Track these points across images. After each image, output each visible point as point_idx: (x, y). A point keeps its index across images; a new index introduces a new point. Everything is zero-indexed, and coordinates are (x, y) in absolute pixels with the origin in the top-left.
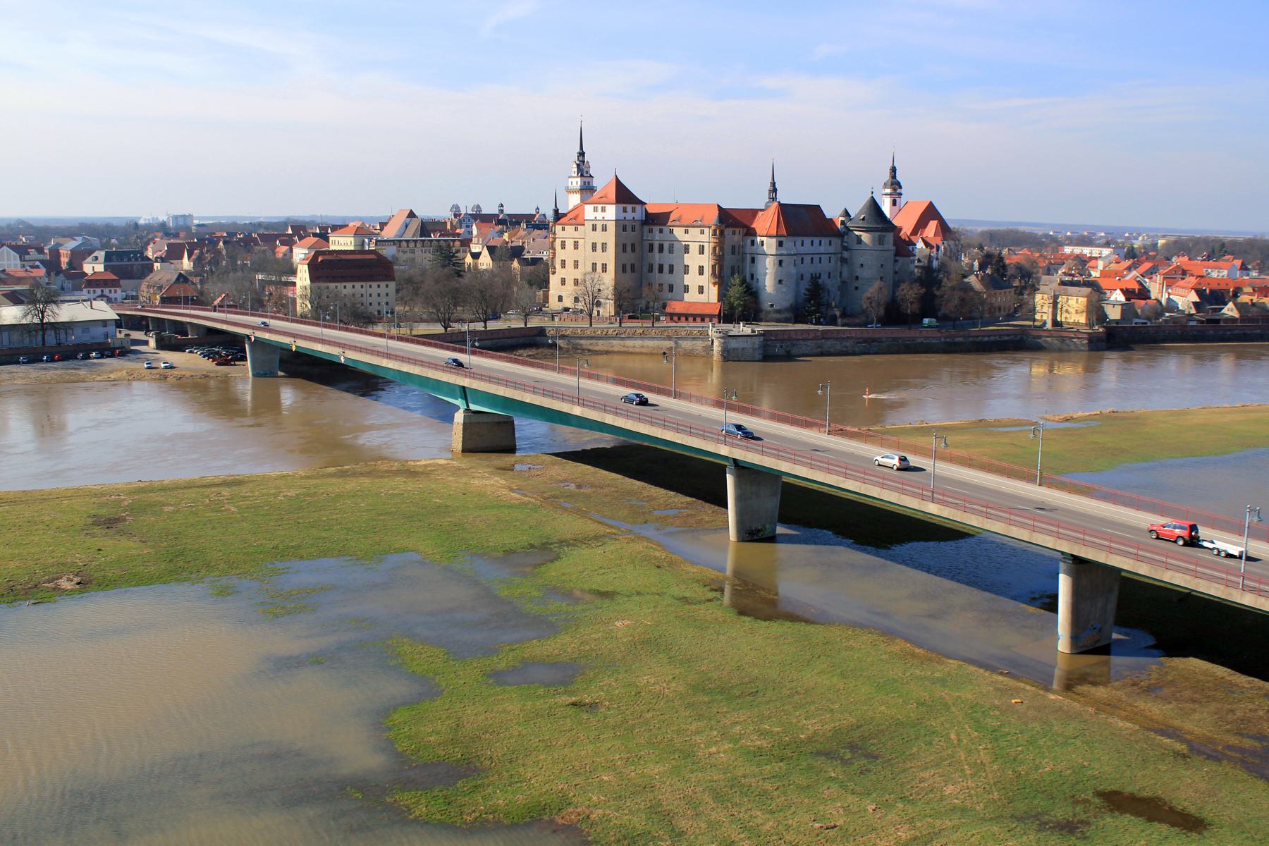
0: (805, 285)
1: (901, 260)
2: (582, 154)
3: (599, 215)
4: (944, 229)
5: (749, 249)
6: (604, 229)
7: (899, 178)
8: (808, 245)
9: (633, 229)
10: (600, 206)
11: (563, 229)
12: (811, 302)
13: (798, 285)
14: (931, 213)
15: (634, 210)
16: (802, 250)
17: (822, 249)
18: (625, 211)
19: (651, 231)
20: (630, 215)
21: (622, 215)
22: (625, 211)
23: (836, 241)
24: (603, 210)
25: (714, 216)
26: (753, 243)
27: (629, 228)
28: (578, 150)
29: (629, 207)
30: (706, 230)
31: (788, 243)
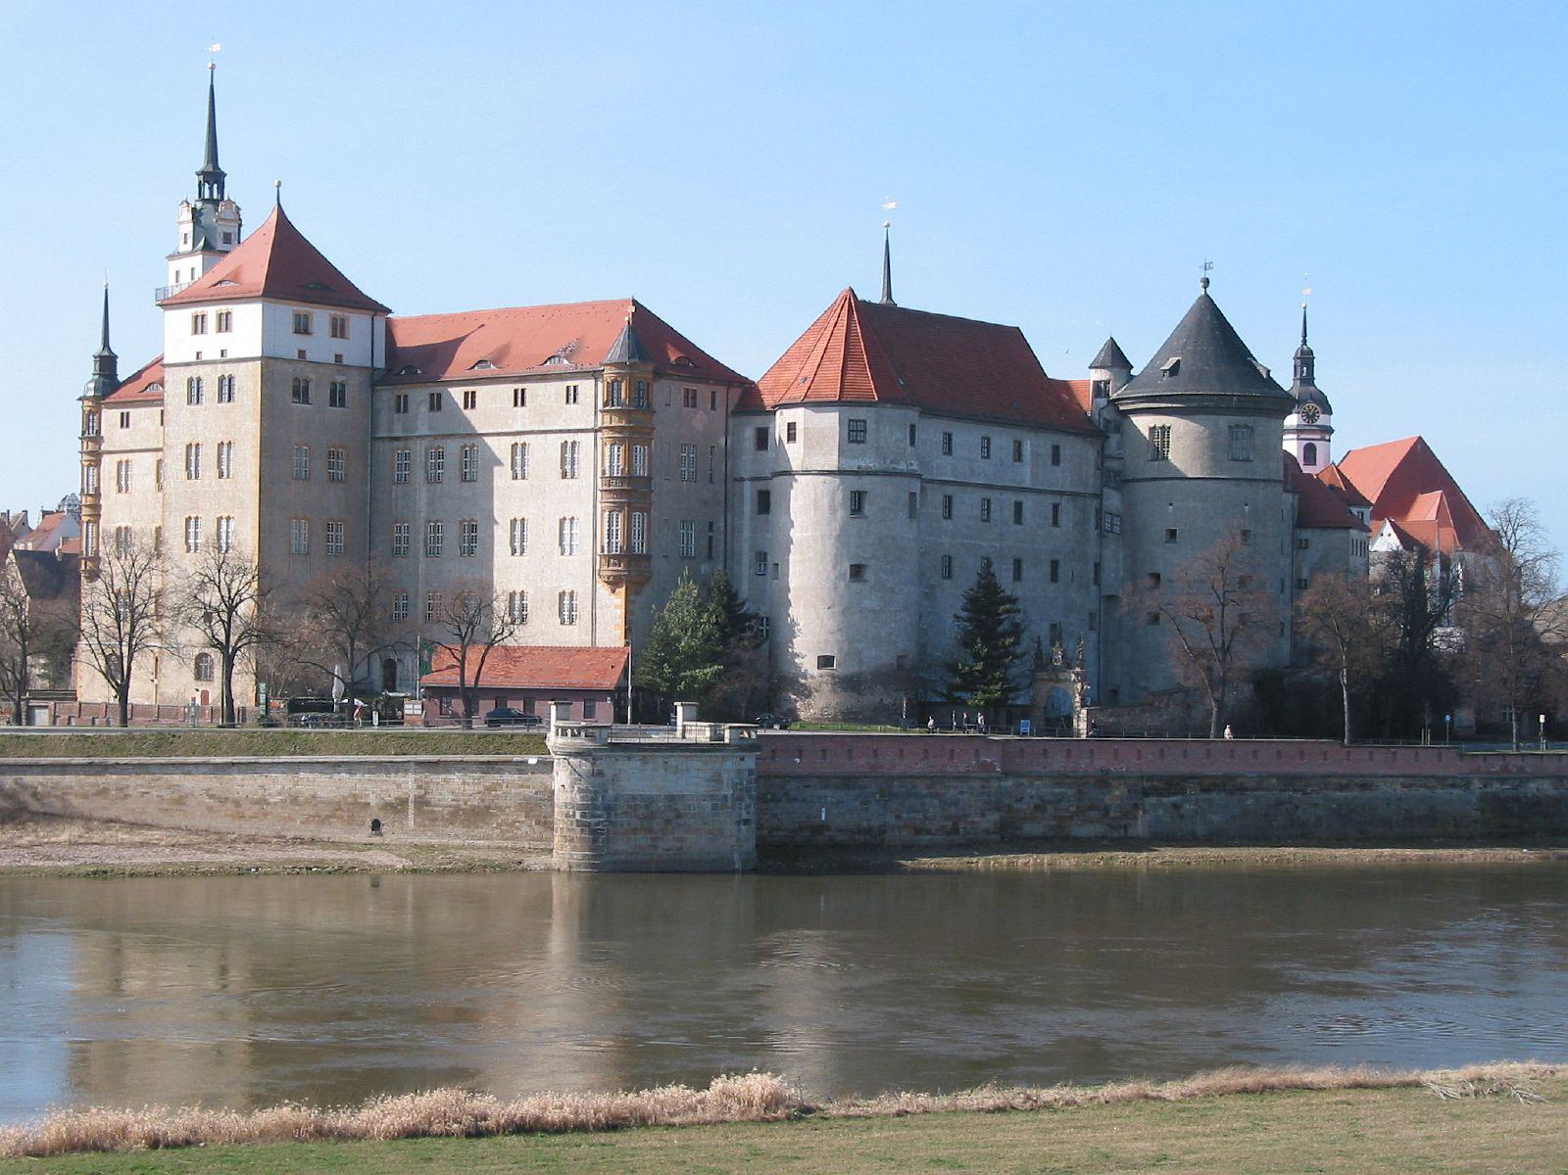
0: (953, 598)
1: (1316, 538)
2: (213, 176)
3: (211, 343)
4: (1460, 511)
5: (748, 462)
6: (227, 389)
7: (1321, 382)
8: (972, 452)
9: (337, 397)
10: (211, 312)
11: (125, 421)
12: (963, 659)
13: (929, 593)
14: (1419, 469)
15: (339, 329)
16: (945, 468)
17: (1025, 474)
18: (302, 327)
19: (402, 406)
20: (321, 346)
21: (290, 345)
22: (302, 327)
23: (1079, 453)
24: (224, 323)
25: (612, 343)
26: (763, 438)
27: (319, 394)
28: (200, 162)
29: (321, 317)
30: (586, 387)
31: (889, 427)
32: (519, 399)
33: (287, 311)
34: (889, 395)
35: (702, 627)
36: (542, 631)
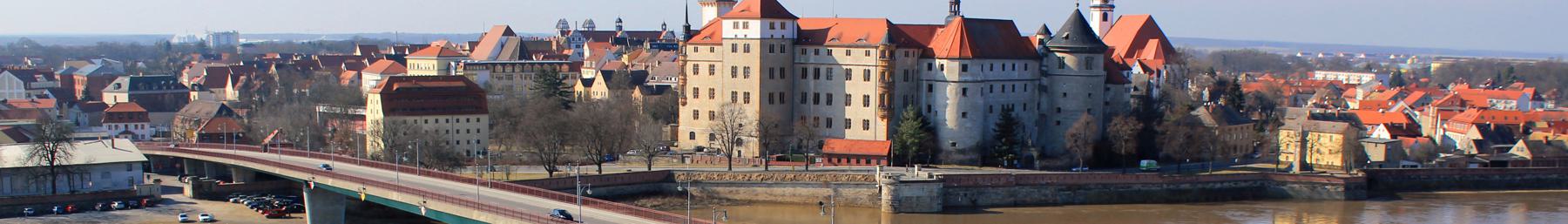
0: (995, 118)
3: (741, 33)
4: (1167, 49)
5: (925, 74)
6: (747, 49)
8: (998, 70)
9: (783, 50)
10: (741, 22)
11: (696, 50)
13: (985, 118)
14: (1150, 29)
15: (783, 26)
16: (991, 75)
17: (1015, 75)
18: (772, 27)
19: (804, 52)
20: (778, 33)
22: (772, 27)
23: (1033, 65)
24: (746, 26)
26: (930, 67)
27: (777, 49)
29: (778, 23)
30: (873, 51)
31: (974, 67)
32: (848, 53)
33: (768, 21)
34: (975, 56)
35: (915, 140)
36: (854, 133)
